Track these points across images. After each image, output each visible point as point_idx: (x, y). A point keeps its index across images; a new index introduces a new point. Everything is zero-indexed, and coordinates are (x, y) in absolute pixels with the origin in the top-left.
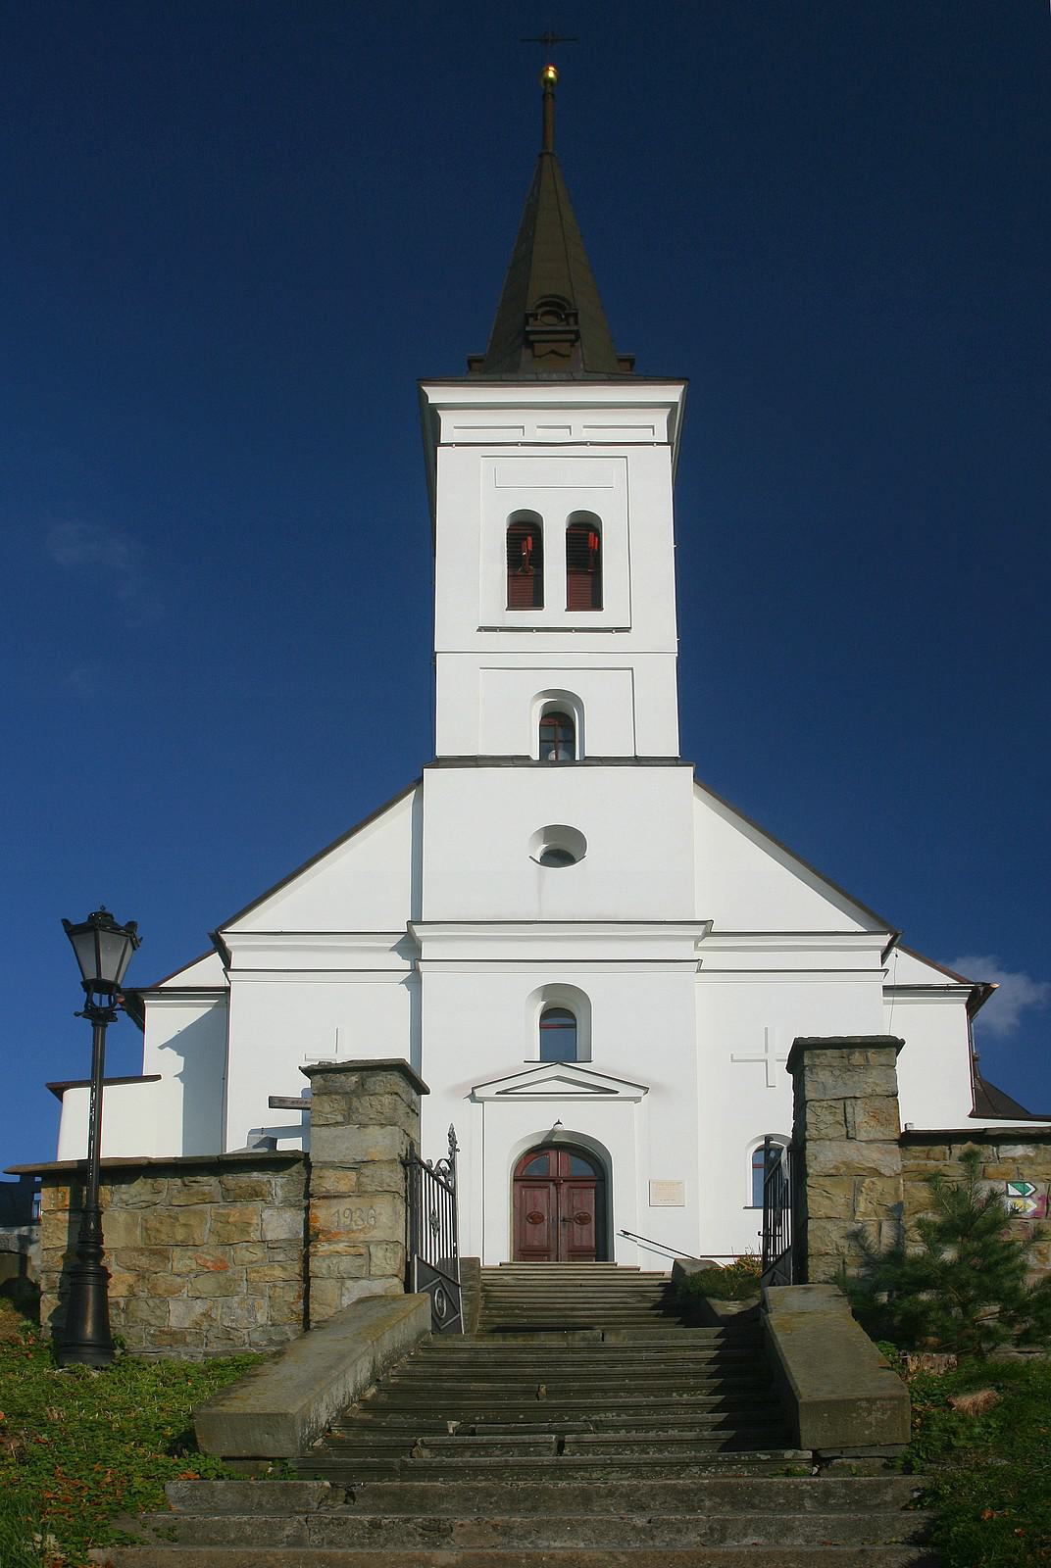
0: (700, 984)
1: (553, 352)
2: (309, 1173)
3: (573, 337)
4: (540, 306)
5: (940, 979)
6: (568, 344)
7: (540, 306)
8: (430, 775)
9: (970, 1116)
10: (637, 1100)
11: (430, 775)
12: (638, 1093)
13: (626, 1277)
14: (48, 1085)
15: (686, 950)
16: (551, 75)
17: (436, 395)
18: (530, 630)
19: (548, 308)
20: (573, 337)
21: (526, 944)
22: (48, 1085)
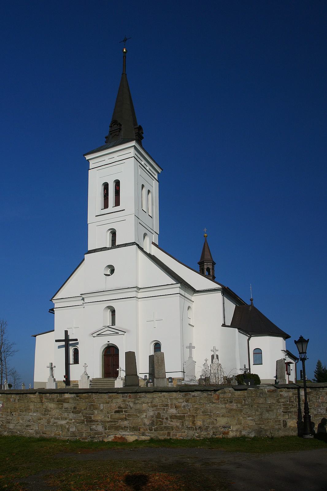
0: (140, 303)
1: (115, 135)
2: (234, 389)
3: (119, 130)
4: (112, 124)
5: (214, 285)
6: (118, 132)
7: (112, 124)
8: (86, 256)
9: (222, 326)
10: (124, 335)
11: (86, 256)
12: (123, 333)
13: (112, 383)
14: (319, 361)
15: (133, 294)
16: (125, 51)
17: (88, 157)
18: (105, 214)
19: (114, 123)
20: (119, 130)
21: (121, 294)
22: (319, 361)
